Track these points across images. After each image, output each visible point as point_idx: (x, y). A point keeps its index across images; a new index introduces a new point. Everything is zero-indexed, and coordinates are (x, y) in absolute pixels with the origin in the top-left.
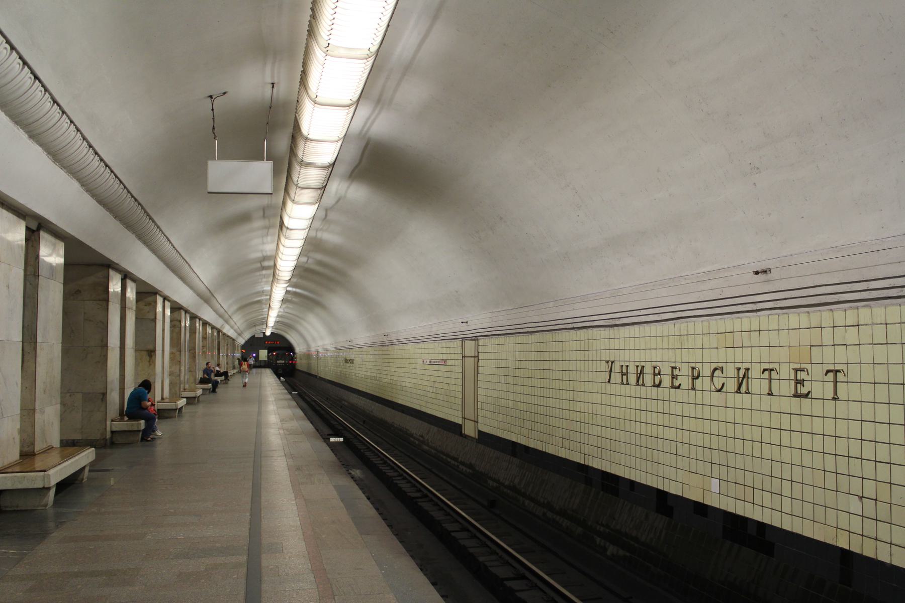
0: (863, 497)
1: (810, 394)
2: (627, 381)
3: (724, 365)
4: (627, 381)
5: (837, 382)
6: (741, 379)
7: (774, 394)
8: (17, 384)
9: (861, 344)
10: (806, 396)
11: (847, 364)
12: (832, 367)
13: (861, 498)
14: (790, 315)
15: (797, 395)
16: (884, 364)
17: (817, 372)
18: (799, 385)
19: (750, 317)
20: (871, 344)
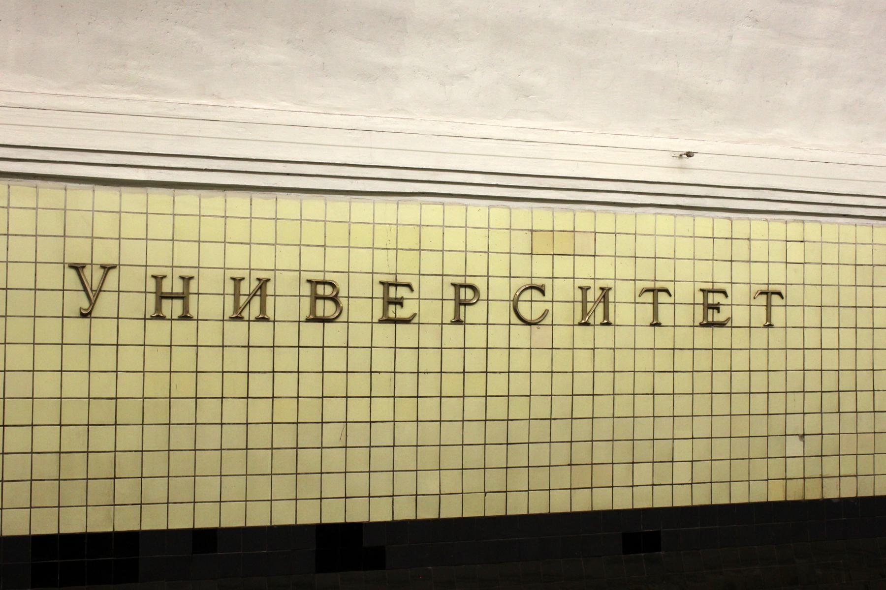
0: (804, 435)
1: (730, 322)
2: (606, 315)
3: (781, 288)
4: (606, 315)
5: (653, 304)
6: (243, 300)
7: (663, 324)
8: (276, 184)
9: (806, 263)
10: (721, 325)
11: (786, 284)
12: (650, 285)
13: (802, 436)
14: (447, 207)
15: (314, 319)
16: (834, 285)
17: (739, 294)
18: (710, 311)
19: (443, 204)
20: (819, 264)
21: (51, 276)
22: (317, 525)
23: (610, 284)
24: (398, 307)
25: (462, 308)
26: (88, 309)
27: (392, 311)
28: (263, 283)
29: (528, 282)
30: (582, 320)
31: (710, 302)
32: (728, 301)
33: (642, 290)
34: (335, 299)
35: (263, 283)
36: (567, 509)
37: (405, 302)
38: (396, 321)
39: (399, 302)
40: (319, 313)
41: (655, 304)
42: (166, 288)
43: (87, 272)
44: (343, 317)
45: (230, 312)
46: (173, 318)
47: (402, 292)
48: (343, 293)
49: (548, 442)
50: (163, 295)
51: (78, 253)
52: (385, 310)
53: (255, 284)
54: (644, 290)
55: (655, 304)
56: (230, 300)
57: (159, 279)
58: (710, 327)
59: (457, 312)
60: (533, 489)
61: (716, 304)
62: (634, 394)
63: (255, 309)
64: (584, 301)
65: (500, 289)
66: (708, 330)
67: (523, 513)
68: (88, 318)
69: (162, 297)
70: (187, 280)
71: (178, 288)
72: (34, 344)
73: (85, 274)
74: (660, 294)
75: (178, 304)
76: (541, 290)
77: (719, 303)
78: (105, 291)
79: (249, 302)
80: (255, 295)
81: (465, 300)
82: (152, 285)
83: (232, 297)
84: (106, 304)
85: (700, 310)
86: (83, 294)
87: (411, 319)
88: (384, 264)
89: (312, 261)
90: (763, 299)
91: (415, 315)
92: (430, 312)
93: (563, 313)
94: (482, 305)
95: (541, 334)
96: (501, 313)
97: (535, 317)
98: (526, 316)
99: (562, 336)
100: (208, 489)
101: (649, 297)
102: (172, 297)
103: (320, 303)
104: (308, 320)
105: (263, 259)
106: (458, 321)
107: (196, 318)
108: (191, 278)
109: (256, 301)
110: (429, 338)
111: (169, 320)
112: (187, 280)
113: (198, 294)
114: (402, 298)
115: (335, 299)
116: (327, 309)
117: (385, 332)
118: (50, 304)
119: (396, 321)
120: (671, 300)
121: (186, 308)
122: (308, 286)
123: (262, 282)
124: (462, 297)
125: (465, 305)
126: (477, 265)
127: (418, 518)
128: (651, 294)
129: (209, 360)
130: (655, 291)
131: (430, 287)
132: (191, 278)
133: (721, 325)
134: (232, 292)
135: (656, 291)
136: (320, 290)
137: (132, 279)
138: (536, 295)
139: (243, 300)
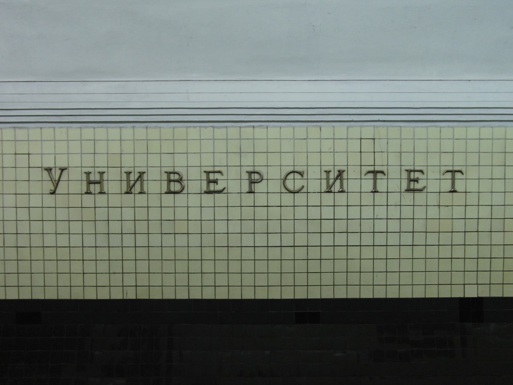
3: (384, 169)
6: (331, 181)
10: (420, 190)
12: (450, 168)
15: (169, 192)
21: (36, 174)
22: (460, 299)
23: (105, 170)
24: (416, 183)
25: (253, 184)
26: (53, 191)
27: (212, 187)
28: (141, 174)
29: (291, 169)
30: (452, 189)
31: (412, 177)
32: (424, 177)
33: (444, 172)
34: (180, 181)
35: (141, 174)
36: (423, 296)
37: (419, 181)
38: (414, 191)
39: (215, 182)
40: (172, 189)
41: (453, 179)
42: (92, 178)
43: (53, 171)
44: (185, 191)
45: (324, 188)
46: (322, 192)
47: (417, 175)
48: (185, 178)
49: (319, 259)
50: (411, 180)
51: (49, 163)
52: (409, 185)
53: (336, 173)
54: (445, 172)
55: (453, 179)
56: (324, 182)
57: (88, 174)
58: (212, 194)
59: (250, 187)
60: (323, 285)
61: (415, 179)
62: (426, 232)
63: (137, 188)
64: (328, 179)
65: (275, 173)
66: (211, 196)
67: (227, 298)
68: (54, 194)
69: (90, 183)
70: (102, 173)
71: (98, 178)
72: (228, 207)
73: (63, 173)
74: (456, 173)
75: (98, 186)
76: (301, 174)
77: (418, 178)
78: (288, 179)
79: (334, 183)
80: (337, 179)
81: (414, 179)
82: (84, 177)
83: (325, 180)
84: (62, 188)
85: (204, 183)
86: (51, 182)
87: (422, 189)
88: (208, 162)
89: (167, 162)
90: (449, 175)
91: (224, 188)
92: (233, 187)
93: (314, 186)
94: (264, 182)
95: (300, 199)
96: (275, 186)
97: (297, 188)
98: (291, 188)
99: (314, 199)
100: (195, 280)
101: (371, 176)
102: (95, 183)
103: (172, 183)
104: (166, 193)
105: (141, 163)
106: (251, 192)
107: (107, 193)
108: (104, 173)
109: (138, 184)
110: (234, 200)
111: (107, 194)
112: (102, 173)
113: (108, 180)
114: (217, 179)
115: (180, 181)
116: (176, 187)
117: (208, 199)
118: (36, 188)
119: (414, 191)
120: (463, 177)
121: (102, 187)
122: (325, 173)
123: (340, 172)
124: (253, 178)
125: (254, 183)
126: (260, 160)
127: (374, 297)
128: (450, 174)
129: (235, 213)
130: (453, 172)
131: (233, 173)
132: (104, 173)
133: (420, 190)
134: (126, 179)
135: (453, 172)
136: (172, 177)
137: (76, 174)
138: (297, 176)
139: (331, 181)
